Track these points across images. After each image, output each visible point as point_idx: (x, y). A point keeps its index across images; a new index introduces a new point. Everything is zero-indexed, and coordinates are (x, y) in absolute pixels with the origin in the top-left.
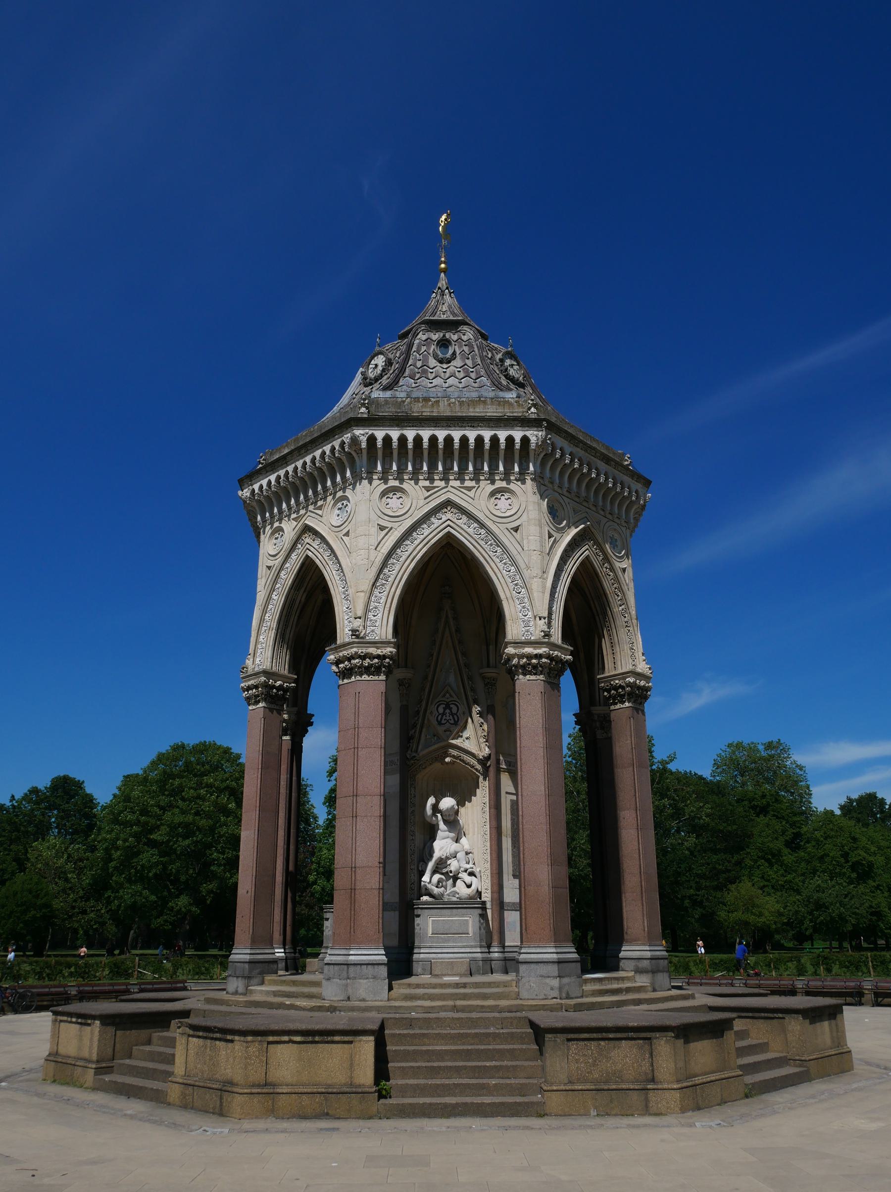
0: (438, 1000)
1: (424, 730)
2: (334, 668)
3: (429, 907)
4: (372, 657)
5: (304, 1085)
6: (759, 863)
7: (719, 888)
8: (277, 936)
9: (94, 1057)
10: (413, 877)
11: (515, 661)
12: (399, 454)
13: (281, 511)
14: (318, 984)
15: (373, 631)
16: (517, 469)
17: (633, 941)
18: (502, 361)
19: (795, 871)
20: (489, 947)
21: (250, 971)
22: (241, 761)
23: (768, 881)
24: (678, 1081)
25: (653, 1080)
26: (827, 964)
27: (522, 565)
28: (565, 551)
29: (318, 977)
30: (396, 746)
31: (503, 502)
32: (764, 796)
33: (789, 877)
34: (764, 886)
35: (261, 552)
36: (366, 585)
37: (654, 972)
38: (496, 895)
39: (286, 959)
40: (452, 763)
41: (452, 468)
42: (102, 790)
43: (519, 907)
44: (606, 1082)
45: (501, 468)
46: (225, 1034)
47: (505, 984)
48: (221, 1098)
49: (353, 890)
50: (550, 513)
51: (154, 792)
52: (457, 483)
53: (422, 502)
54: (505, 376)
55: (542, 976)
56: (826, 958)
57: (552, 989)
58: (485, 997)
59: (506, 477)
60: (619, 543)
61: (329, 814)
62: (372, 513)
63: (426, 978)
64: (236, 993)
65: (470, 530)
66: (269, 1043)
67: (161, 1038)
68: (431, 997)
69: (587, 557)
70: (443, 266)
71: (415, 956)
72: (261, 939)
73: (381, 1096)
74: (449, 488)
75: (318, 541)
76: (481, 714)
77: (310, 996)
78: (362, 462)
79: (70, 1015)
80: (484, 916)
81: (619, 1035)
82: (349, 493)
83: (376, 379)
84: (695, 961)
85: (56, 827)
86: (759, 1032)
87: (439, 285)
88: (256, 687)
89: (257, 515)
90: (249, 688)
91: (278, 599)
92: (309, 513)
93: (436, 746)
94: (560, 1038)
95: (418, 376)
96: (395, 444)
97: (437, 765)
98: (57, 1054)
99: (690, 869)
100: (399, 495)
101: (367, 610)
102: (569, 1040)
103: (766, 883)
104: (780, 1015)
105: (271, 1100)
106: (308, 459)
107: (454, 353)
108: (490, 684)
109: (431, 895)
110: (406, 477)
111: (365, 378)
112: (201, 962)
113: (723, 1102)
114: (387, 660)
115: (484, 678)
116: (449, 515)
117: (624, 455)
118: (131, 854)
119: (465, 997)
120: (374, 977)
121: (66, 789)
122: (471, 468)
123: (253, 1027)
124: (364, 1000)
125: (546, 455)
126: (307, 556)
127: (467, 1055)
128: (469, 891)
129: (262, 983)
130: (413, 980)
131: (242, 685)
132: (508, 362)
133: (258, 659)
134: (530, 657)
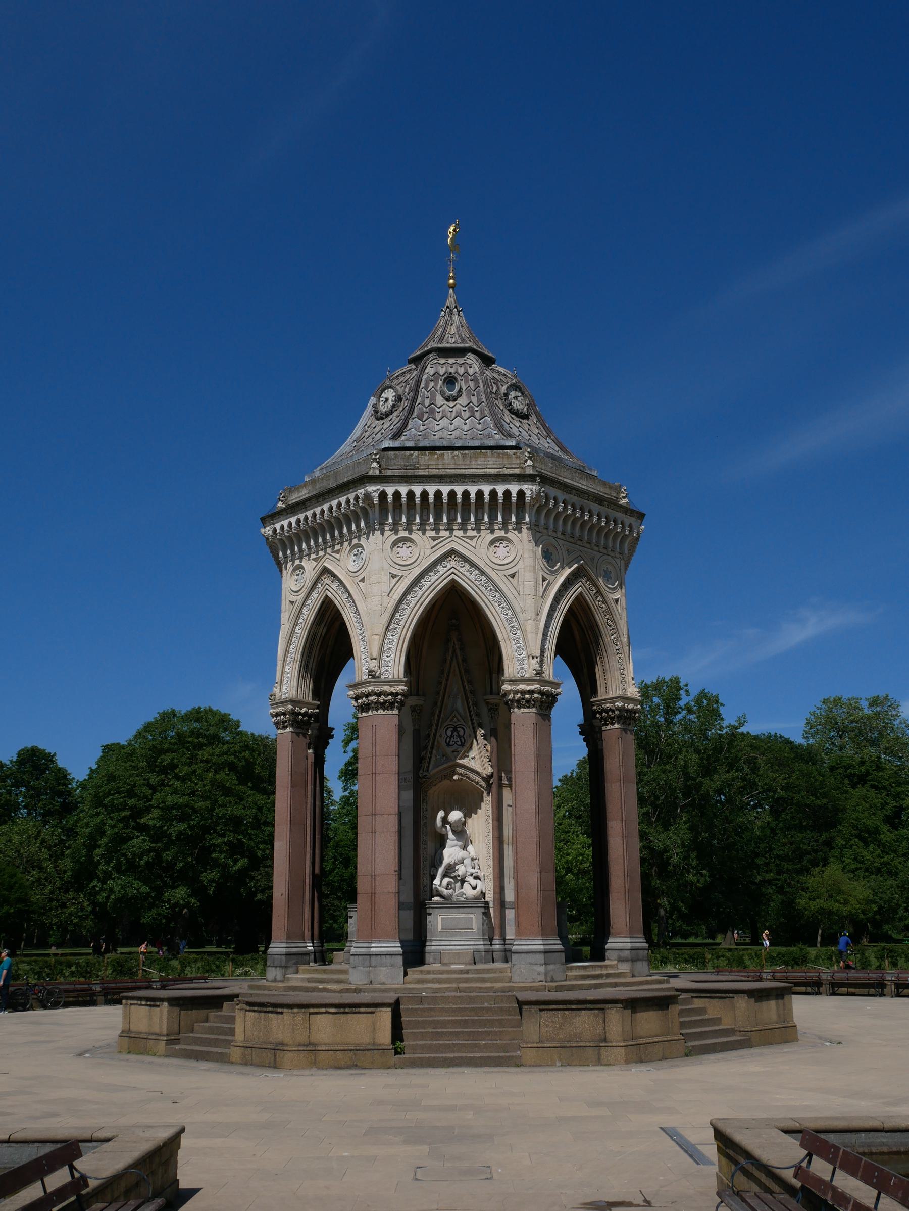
0: (445, 983)
1: (434, 751)
2: (354, 702)
3: (439, 906)
4: (386, 694)
5: (338, 1045)
6: (852, 842)
7: (800, 872)
8: (307, 933)
9: (165, 1032)
10: (425, 880)
11: (510, 696)
12: (408, 506)
13: (301, 550)
14: (345, 972)
15: (387, 670)
16: (514, 519)
17: (618, 935)
18: (506, 395)
19: (895, 852)
20: (491, 940)
21: (287, 962)
22: (241, 729)
23: (862, 862)
24: (624, 1041)
25: (605, 1040)
26: (892, 958)
27: (518, 609)
28: (559, 591)
29: (344, 966)
30: (409, 766)
31: (502, 551)
32: (862, 763)
33: (886, 858)
34: (857, 869)
35: (284, 586)
36: (380, 629)
37: (633, 960)
38: (498, 896)
39: (315, 952)
40: (460, 780)
41: (456, 519)
42: (78, 763)
43: (516, 906)
44: (569, 1041)
45: (500, 519)
46: (276, 1007)
47: (501, 971)
48: (275, 1056)
49: (373, 894)
50: (544, 557)
51: (142, 768)
52: (460, 533)
53: (429, 551)
54: (510, 410)
55: (530, 964)
56: (891, 951)
57: (539, 974)
58: (483, 980)
59: (505, 527)
60: (613, 575)
61: (345, 790)
62: (384, 561)
63: (437, 966)
64: (275, 980)
65: (472, 577)
66: (310, 1013)
67: (217, 1016)
68: (439, 981)
69: (581, 593)
70: (451, 281)
71: (427, 948)
72: (293, 936)
73: (397, 1053)
74: (453, 538)
75: (336, 583)
76: (485, 737)
77: (339, 982)
78: (375, 514)
79: (140, 999)
80: (486, 914)
81: (579, 1006)
82: (363, 541)
83: (387, 415)
84: (750, 955)
85: (25, 807)
86: (714, 1008)
87: (448, 303)
88: (284, 714)
89: (281, 550)
90: (277, 715)
91: (301, 633)
92: (327, 556)
93: (445, 765)
94: (535, 1008)
95: (426, 416)
96: (404, 499)
97: (446, 782)
98: (129, 1031)
99: (771, 850)
100: (408, 544)
101: (381, 651)
102: (541, 1010)
103: (859, 865)
104: (731, 995)
105: (312, 1055)
106: (326, 507)
107: (460, 391)
108: (493, 709)
109: (441, 896)
110: (414, 528)
111: (376, 412)
112: (211, 959)
113: (664, 1058)
114: (400, 697)
115: (487, 704)
116: (453, 563)
117: (620, 486)
118: (120, 840)
119: (467, 980)
120: (392, 965)
121: (35, 761)
122: (472, 519)
123: (298, 1002)
124: (384, 984)
125: (540, 505)
126: (327, 596)
127: (465, 1023)
128: (474, 892)
129: (297, 972)
130: (425, 968)
131: (272, 711)
132: (513, 394)
133: (284, 688)
134: (523, 693)
